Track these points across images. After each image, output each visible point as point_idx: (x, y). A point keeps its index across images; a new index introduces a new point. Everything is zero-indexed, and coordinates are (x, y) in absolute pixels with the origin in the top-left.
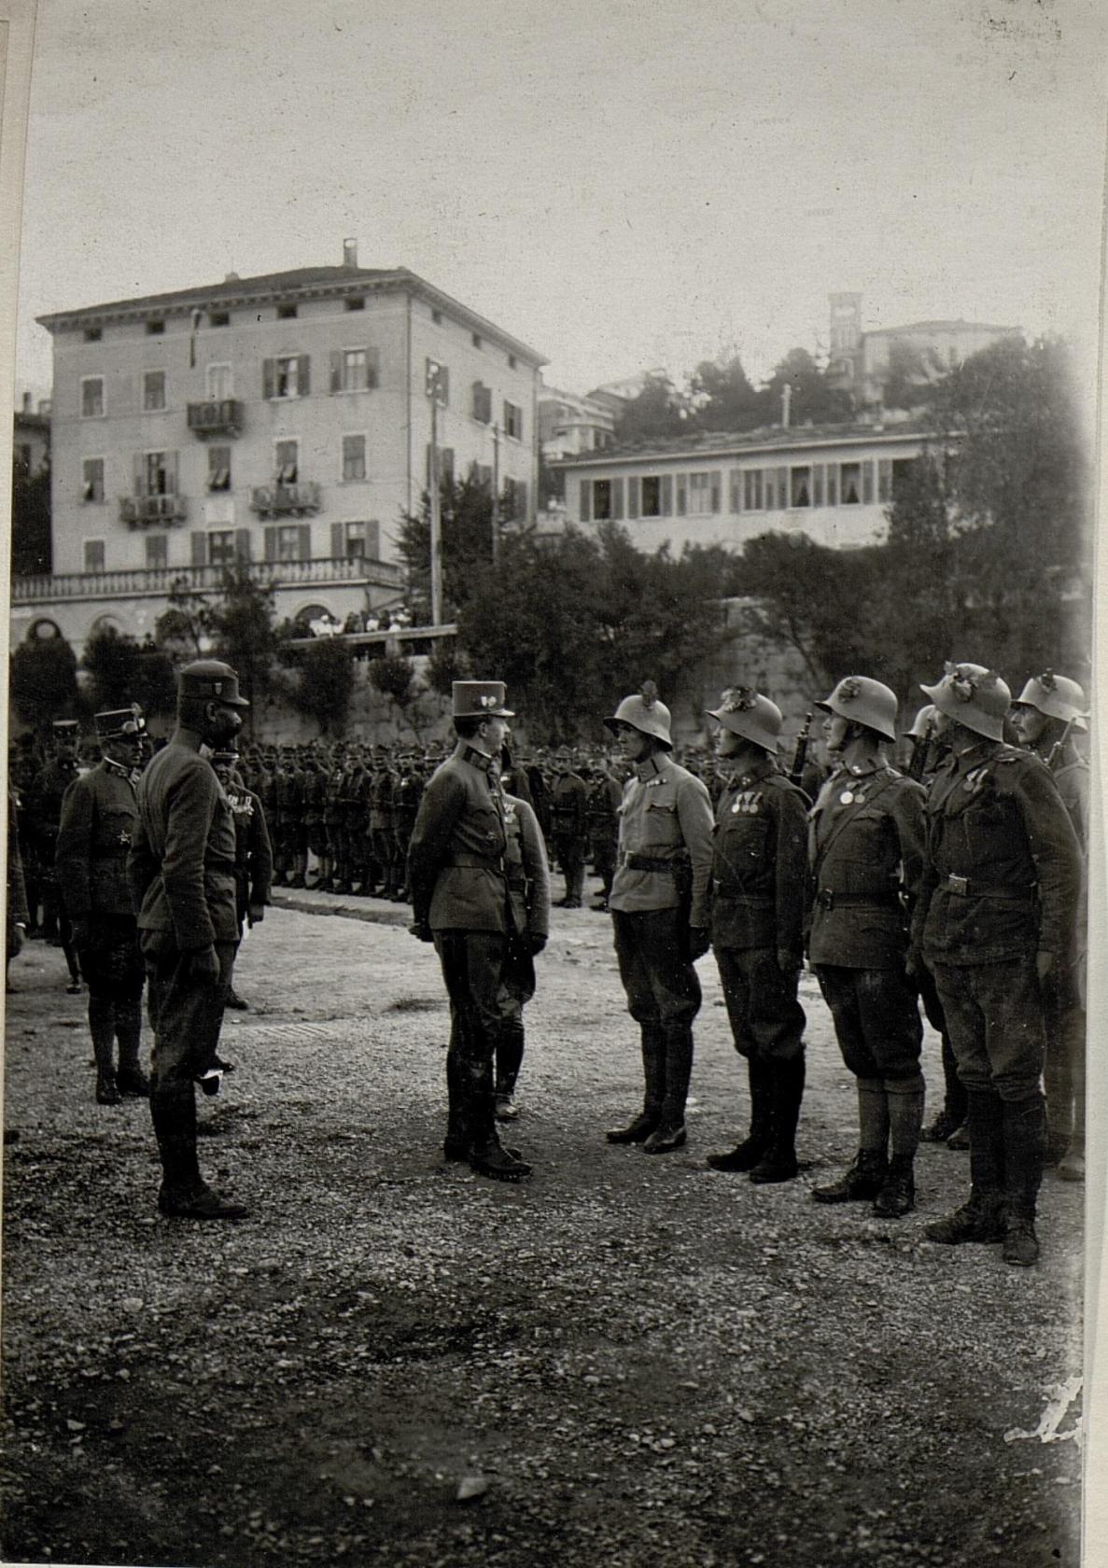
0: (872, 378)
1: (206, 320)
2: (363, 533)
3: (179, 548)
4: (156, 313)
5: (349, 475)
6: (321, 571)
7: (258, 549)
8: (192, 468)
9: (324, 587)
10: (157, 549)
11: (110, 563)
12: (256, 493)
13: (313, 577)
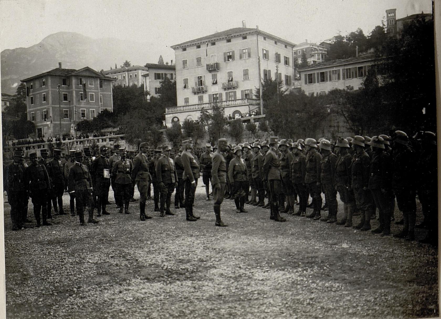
0: (399, 32)
1: (210, 44)
2: (249, 92)
3: (206, 98)
4: (198, 43)
5: (245, 78)
6: (238, 102)
7: (224, 98)
8: (208, 79)
9: (239, 106)
10: (201, 99)
11: (190, 103)
12: (223, 84)
13: (236, 104)
